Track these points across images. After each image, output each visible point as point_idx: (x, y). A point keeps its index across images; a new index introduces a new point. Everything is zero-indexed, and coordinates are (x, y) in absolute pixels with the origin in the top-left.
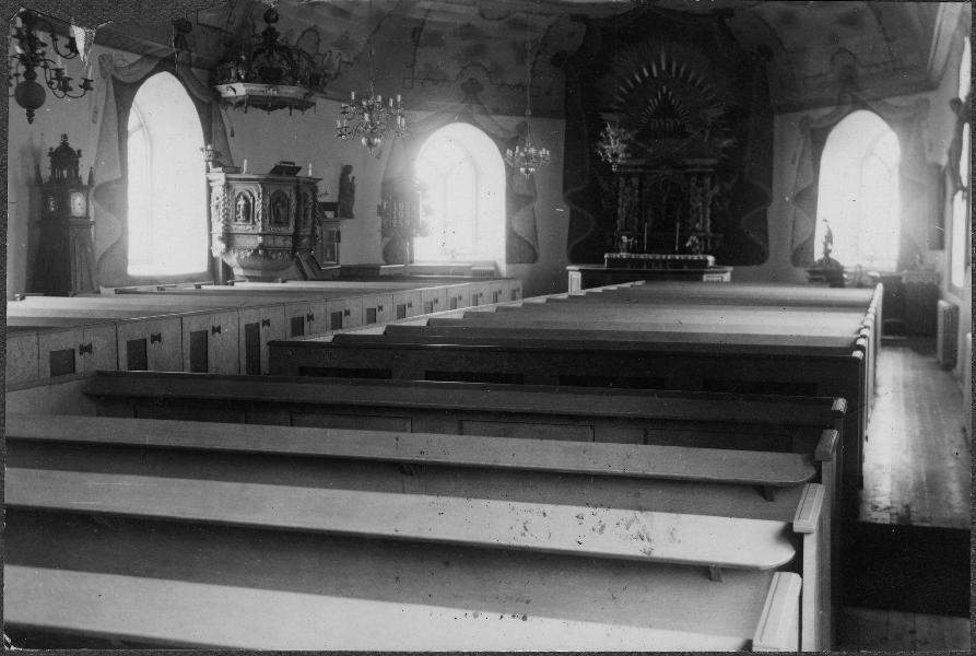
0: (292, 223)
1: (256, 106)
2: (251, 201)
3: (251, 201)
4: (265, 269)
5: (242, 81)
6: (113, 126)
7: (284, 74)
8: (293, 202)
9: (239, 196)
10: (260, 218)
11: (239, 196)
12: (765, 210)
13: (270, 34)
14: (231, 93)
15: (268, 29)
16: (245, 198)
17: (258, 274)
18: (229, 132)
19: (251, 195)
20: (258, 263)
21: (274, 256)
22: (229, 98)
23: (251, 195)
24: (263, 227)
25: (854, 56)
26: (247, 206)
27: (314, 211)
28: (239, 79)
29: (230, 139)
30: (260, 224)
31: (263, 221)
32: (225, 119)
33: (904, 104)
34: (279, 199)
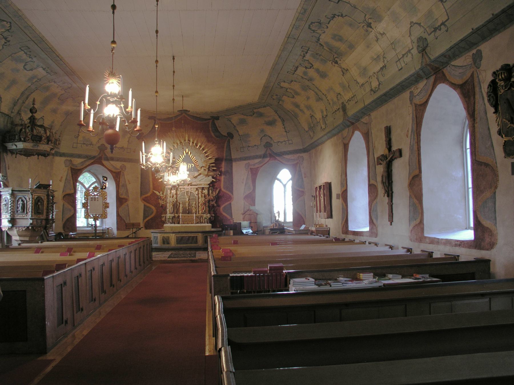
0: (45, 213)
1: (21, 154)
2: (25, 202)
3: (25, 202)
4: (31, 237)
5: (23, 141)
6: (113, 170)
7: (43, 138)
8: (45, 202)
9: (19, 199)
10: (30, 210)
11: (19, 199)
12: (230, 204)
13: (32, 120)
14: (14, 147)
15: (31, 116)
16: (22, 200)
17: (27, 239)
18: (7, 166)
19: (25, 199)
20: (29, 233)
21: (36, 230)
22: (13, 150)
23: (25, 199)
24: (32, 215)
25: (271, 138)
26: (23, 205)
27: (199, 211)
28: (20, 140)
29: (7, 170)
30: (30, 213)
31: (32, 212)
32: (6, 161)
33: (292, 158)
34: (39, 201)
